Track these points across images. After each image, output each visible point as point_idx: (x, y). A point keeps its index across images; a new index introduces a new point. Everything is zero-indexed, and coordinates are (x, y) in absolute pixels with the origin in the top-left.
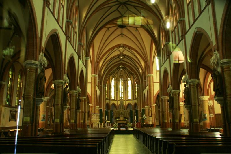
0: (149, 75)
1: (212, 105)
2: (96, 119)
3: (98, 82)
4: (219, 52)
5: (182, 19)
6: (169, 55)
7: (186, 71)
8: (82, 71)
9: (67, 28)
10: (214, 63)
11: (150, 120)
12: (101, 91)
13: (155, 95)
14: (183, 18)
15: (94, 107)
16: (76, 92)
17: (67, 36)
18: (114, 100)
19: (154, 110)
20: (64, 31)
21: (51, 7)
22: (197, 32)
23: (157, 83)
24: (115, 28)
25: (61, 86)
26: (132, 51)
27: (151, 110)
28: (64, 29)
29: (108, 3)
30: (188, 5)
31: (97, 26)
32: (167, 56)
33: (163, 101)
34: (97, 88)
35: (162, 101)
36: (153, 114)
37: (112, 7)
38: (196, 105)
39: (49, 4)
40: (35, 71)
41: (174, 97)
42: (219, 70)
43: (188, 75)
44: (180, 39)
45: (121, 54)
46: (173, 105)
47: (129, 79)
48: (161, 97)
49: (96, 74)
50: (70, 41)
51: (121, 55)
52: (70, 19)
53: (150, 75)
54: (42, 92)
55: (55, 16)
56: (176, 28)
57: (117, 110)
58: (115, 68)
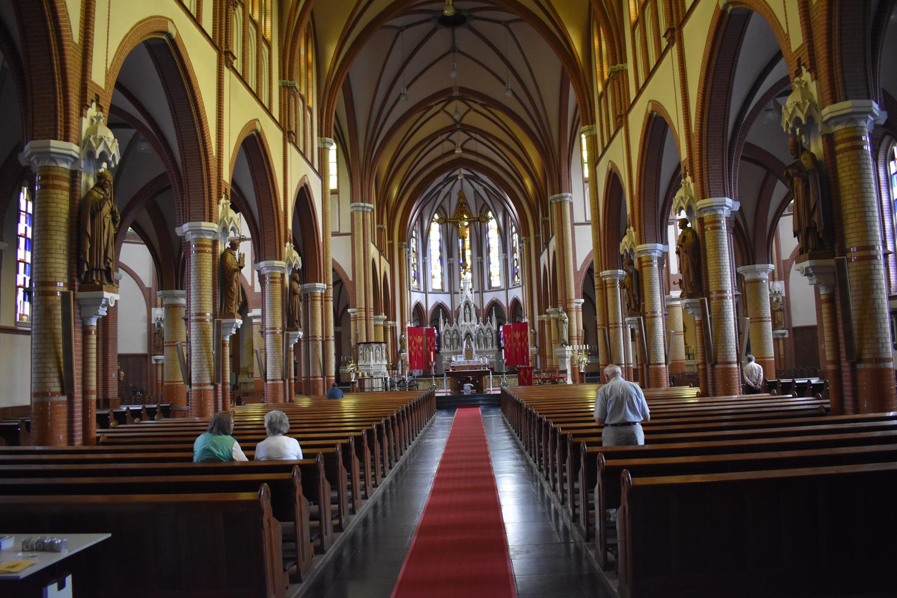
0: (557, 196)
1: (784, 295)
3: (380, 230)
4: (816, 73)
7: (688, 168)
8: (304, 194)
9: (221, 19)
10: (797, 121)
12: (391, 262)
13: (582, 269)
21: (237, 64)
23: (586, 223)
24: (430, 26)
25: (210, 244)
26: (493, 114)
27: (567, 320)
32: (616, 118)
33: (606, 288)
34: (373, 251)
35: (603, 286)
36: (575, 334)
38: (725, 298)
39: (231, 59)
41: (645, 270)
42: (817, 147)
43: (693, 181)
44: (664, 43)
45: (454, 125)
47: (490, 214)
48: (598, 273)
50: (243, 73)
54: (103, 267)
57: (451, 326)
58: (440, 179)
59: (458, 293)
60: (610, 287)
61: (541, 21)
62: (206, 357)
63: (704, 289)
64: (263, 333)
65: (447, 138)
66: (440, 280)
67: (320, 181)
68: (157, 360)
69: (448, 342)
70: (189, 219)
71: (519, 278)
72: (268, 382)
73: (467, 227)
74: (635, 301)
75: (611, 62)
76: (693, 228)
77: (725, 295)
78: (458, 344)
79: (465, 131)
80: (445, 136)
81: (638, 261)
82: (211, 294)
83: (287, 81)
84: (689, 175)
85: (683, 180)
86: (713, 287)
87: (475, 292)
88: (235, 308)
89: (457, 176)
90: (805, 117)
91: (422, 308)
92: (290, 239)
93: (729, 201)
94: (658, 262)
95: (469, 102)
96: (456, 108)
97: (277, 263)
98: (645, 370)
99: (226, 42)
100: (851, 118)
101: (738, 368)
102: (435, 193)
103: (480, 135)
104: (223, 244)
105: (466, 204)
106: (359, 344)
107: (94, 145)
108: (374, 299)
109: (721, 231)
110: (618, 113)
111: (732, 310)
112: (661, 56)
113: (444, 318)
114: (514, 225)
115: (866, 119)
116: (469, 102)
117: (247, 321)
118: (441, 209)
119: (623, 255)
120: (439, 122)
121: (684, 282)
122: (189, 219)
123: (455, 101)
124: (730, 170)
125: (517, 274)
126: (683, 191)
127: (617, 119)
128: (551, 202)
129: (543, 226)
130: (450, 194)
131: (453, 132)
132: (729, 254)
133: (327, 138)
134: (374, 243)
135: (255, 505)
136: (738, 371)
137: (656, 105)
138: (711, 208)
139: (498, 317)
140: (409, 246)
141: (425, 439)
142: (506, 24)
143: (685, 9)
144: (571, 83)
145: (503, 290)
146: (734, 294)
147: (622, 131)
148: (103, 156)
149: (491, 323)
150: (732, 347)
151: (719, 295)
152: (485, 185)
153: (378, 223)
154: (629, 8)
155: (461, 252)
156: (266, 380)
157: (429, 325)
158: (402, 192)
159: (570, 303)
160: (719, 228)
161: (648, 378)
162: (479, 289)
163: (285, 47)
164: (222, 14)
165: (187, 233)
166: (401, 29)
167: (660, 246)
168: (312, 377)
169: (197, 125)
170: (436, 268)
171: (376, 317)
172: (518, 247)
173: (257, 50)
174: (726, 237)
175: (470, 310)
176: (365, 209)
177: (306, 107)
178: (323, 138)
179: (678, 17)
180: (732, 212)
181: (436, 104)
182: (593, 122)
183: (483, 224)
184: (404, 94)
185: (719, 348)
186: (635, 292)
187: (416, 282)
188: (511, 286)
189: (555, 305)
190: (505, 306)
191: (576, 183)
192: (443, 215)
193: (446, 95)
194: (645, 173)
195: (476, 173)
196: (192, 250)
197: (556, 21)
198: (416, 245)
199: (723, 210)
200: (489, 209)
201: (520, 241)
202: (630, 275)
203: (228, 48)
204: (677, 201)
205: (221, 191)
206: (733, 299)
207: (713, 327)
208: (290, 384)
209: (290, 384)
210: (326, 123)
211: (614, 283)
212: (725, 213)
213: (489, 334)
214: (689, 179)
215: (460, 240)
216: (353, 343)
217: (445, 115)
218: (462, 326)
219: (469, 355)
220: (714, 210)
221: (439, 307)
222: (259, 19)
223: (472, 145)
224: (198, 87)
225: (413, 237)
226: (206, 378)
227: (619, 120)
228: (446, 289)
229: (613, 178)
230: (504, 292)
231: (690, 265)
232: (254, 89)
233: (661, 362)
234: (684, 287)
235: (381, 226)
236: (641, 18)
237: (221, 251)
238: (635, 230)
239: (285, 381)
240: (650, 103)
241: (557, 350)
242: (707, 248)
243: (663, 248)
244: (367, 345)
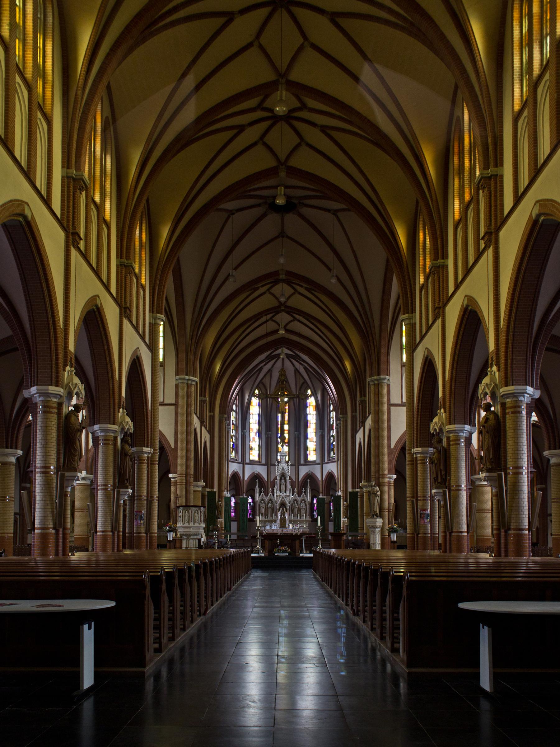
0: (375, 377)
2: (192, 524)
3: (203, 402)
5: (490, 171)
7: (494, 358)
8: (136, 363)
9: (121, 290)
11: (375, 527)
12: (211, 432)
14: (495, 169)
15: (187, 485)
18: (258, 463)
20: (58, 214)
21: (82, 245)
22: (539, 216)
23: (402, 405)
24: (256, 212)
25: (56, 405)
27: (379, 493)
28: (56, 205)
29: (254, 187)
30: (516, 118)
31: (188, 201)
32: (435, 309)
33: (417, 464)
34: (196, 422)
35: (414, 462)
37: (241, 129)
38: (522, 473)
39: (78, 240)
40: (146, 462)
41: (452, 448)
43: (499, 370)
45: (279, 307)
47: (309, 392)
51: (282, 311)
52: (128, 258)
55: (38, 185)
57: (266, 495)
58: (263, 356)
60: (420, 463)
61: (369, 213)
62: (49, 505)
63: (503, 465)
65: (271, 319)
66: (258, 452)
67: (150, 354)
69: (263, 510)
70: (37, 382)
71: (334, 454)
72: (98, 534)
73: (286, 403)
75: (482, 168)
76: (496, 412)
77: (521, 471)
78: (273, 512)
79: (288, 313)
80: (269, 316)
81: (447, 440)
82: (56, 450)
83: (124, 260)
84: (495, 365)
85: (489, 369)
87: (291, 465)
89: (279, 355)
91: (239, 477)
92: (123, 405)
93: (530, 390)
94: (465, 441)
95: (294, 286)
97: (111, 427)
98: (448, 537)
99: (73, 224)
101: (529, 535)
102: (257, 369)
103: (304, 317)
104: (67, 407)
105: (287, 381)
106: (179, 507)
108: (194, 467)
109: (521, 415)
110: (436, 305)
111: (527, 484)
112: (479, 255)
113: (260, 487)
114: (332, 403)
116: (294, 286)
118: (261, 385)
119: (433, 433)
121: (484, 458)
122: (37, 382)
123: (281, 284)
124: (533, 361)
125: (333, 450)
126: (489, 379)
127: (435, 311)
128: (369, 384)
129: (361, 405)
130: (271, 371)
131: (277, 313)
132: (527, 435)
133: (158, 315)
134: (196, 414)
136: (529, 538)
137: (470, 299)
138: (513, 395)
139: (312, 490)
140: (229, 418)
141: (244, 586)
142: (335, 212)
143: (503, 214)
144: (394, 274)
146: (530, 470)
149: (306, 494)
150: (524, 516)
152: (306, 365)
153: (201, 396)
154: (454, 208)
155: (279, 426)
156: (96, 532)
157: (245, 494)
158: (224, 368)
159: (383, 478)
160: (520, 412)
161: (450, 544)
162: (295, 462)
163: (123, 227)
164: (70, 197)
165: (35, 396)
166: (231, 213)
167: (468, 427)
168: (136, 533)
169: (47, 299)
171: (195, 483)
172: (335, 424)
173: (98, 230)
174: (525, 421)
175: (286, 481)
178: (154, 315)
179: (496, 222)
180: (532, 399)
181: (262, 286)
182: (413, 311)
183: (302, 401)
184: (232, 275)
185: (513, 516)
186: (442, 467)
188: (326, 461)
189: (368, 480)
190: (320, 479)
191: (395, 368)
192: (264, 391)
194: (458, 361)
195: (298, 353)
196: (38, 410)
197: (384, 213)
199: (524, 396)
201: (337, 419)
202: (439, 452)
203: (75, 229)
205: (67, 360)
206: (528, 474)
207: (508, 497)
208: (118, 536)
209: (118, 536)
210: (157, 300)
211: (424, 460)
212: (526, 399)
213: (303, 505)
214: (495, 368)
215: (279, 415)
217: (271, 297)
218: (277, 496)
219: (283, 524)
220: (516, 397)
221: (256, 477)
222: (100, 201)
223: (295, 326)
224: (49, 265)
225: (233, 411)
226: (49, 523)
227: (437, 311)
228: (263, 461)
229: (429, 364)
230: (319, 467)
231: (491, 445)
233: (463, 530)
234: (484, 462)
235: (203, 398)
236: (475, 198)
237: (66, 412)
238: (445, 412)
239: (113, 533)
240: (466, 298)
241: (368, 521)
242: (507, 429)
243: (471, 429)
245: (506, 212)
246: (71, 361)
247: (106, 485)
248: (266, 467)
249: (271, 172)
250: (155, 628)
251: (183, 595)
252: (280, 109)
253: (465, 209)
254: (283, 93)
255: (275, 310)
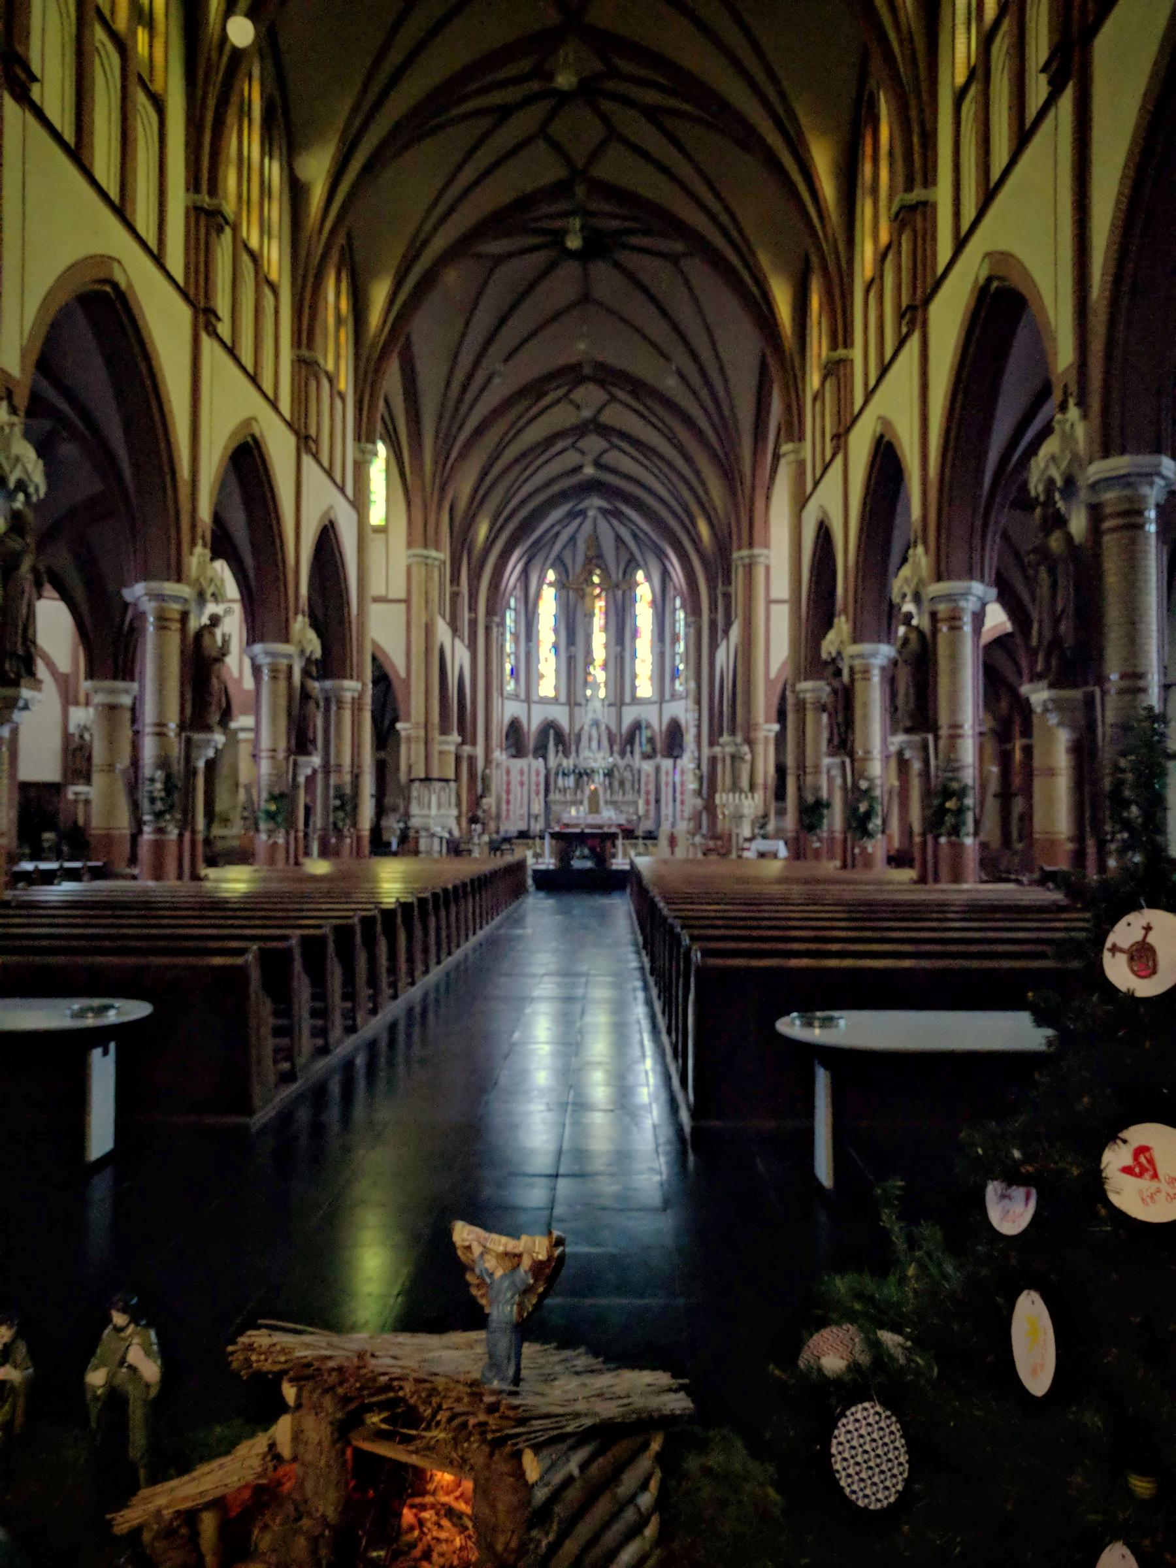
3: (455, 596)
5: (917, 194)
6: (842, 430)
10: (1051, 481)
12: (472, 647)
13: (778, 677)
16: (289, 656)
17: (202, 305)
18: (555, 701)
19: (766, 767)
21: (224, 329)
22: (989, 280)
25: (177, 616)
27: (748, 757)
30: (960, 97)
34: (443, 631)
35: (801, 706)
36: (760, 780)
42: (1078, 524)
46: (846, 732)
49: (437, 548)
50: (233, 341)
53: (751, 557)
54: (21, 651)
56: (890, 257)
59: (580, 705)
64: (255, 756)
68: (76, 794)
74: (840, 735)
80: (568, 441)
83: (305, 353)
86: (943, 719)
88: (215, 718)
90: (1062, 474)
96: (589, 396)
100: (1123, 480)
106: (412, 781)
107: (7, 468)
112: (901, 343)
113: (556, 745)
115: (1151, 484)
117: (232, 737)
118: (560, 564)
120: (561, 417)
131: (582, 435)
134: (444, 617)
135: (242, 971)
137: (885, 422)
138: (950, 597)
140: (502, 624)
145: (655, 703)
147: (839, 460)
148: (21, 486)
151: (952, 732)
170: (548, 664)
171: (443, 738)
176: (430, 561)
177: (335, 392)
178: (363, 445)
182: (801, 438)
187: (512, 683)
189: (733, 732)
193: (572, 375)
198: (516, 622)
199: (967, 600)
200: (638, 567)
201: (687, 625)
204: (1042, 465)
213: (628, 775)
216: (403, 777)
219: (594, 808)
223: (613, 458)
228: (563, 698)
229: (824, 534)
232: (250, 369)
244: (427, 783)
245: (940, 269)
246: (203, 538)
247: (274, 750)
248: (566, 709)
249: (561, 189)
250: (314, 1014)
251: (410, 937)
252: (564, 80)
253: (881, 258)
254: (569, 52)
255: (581, 430)
